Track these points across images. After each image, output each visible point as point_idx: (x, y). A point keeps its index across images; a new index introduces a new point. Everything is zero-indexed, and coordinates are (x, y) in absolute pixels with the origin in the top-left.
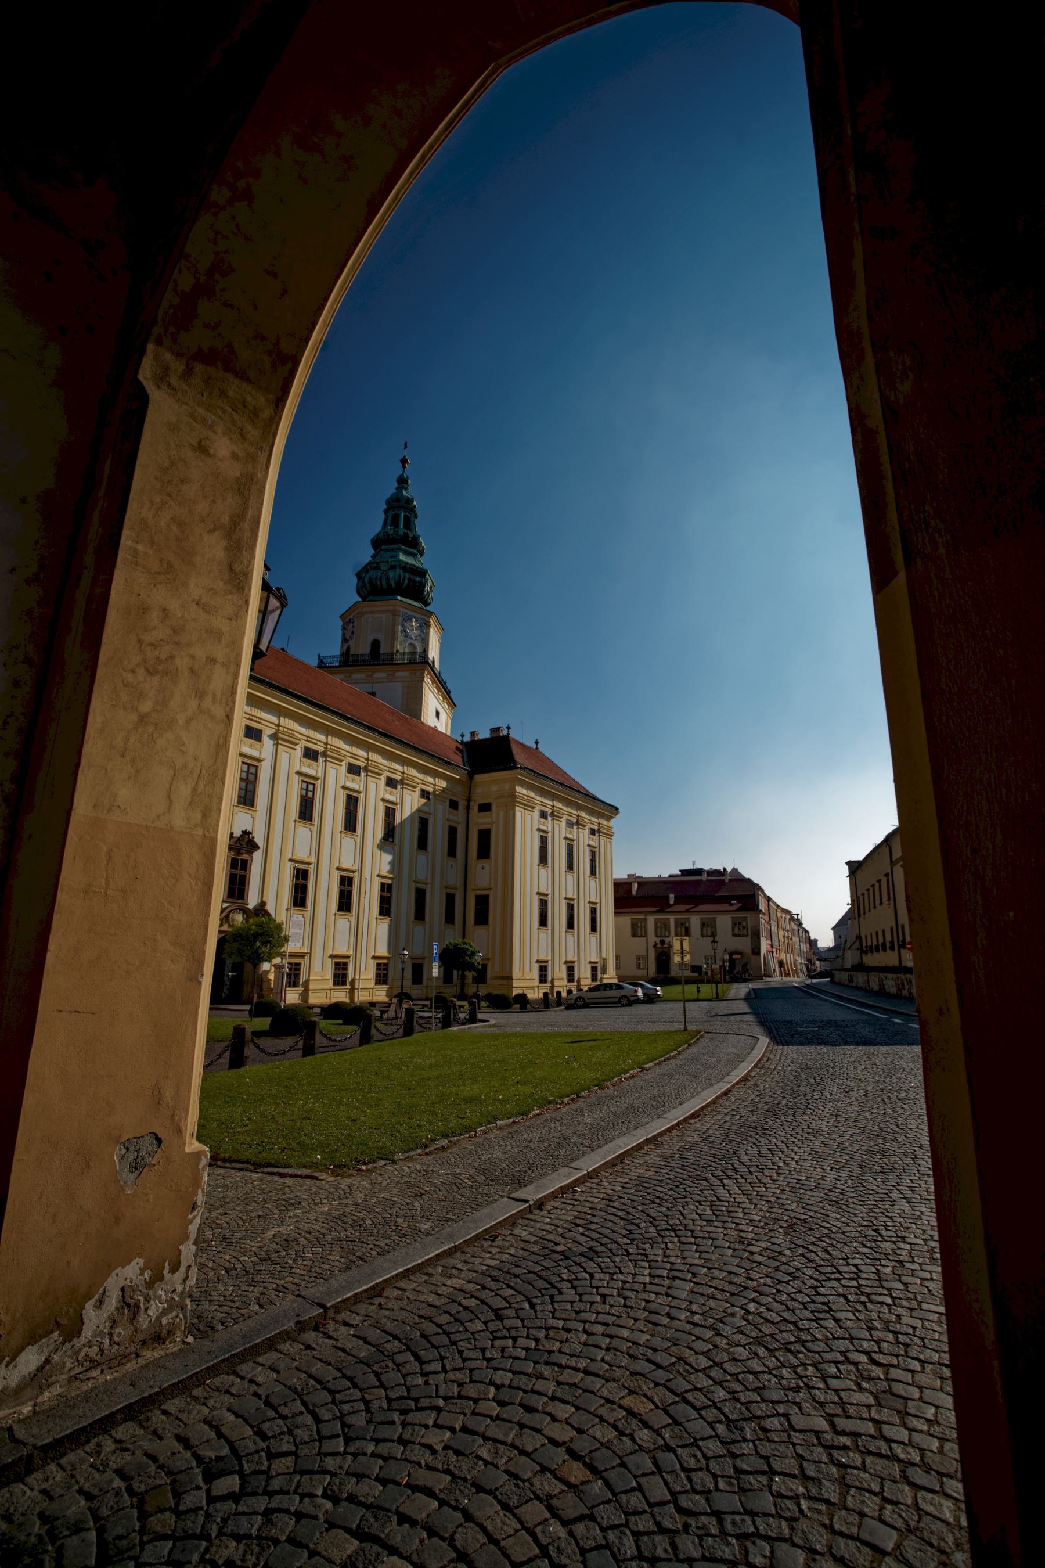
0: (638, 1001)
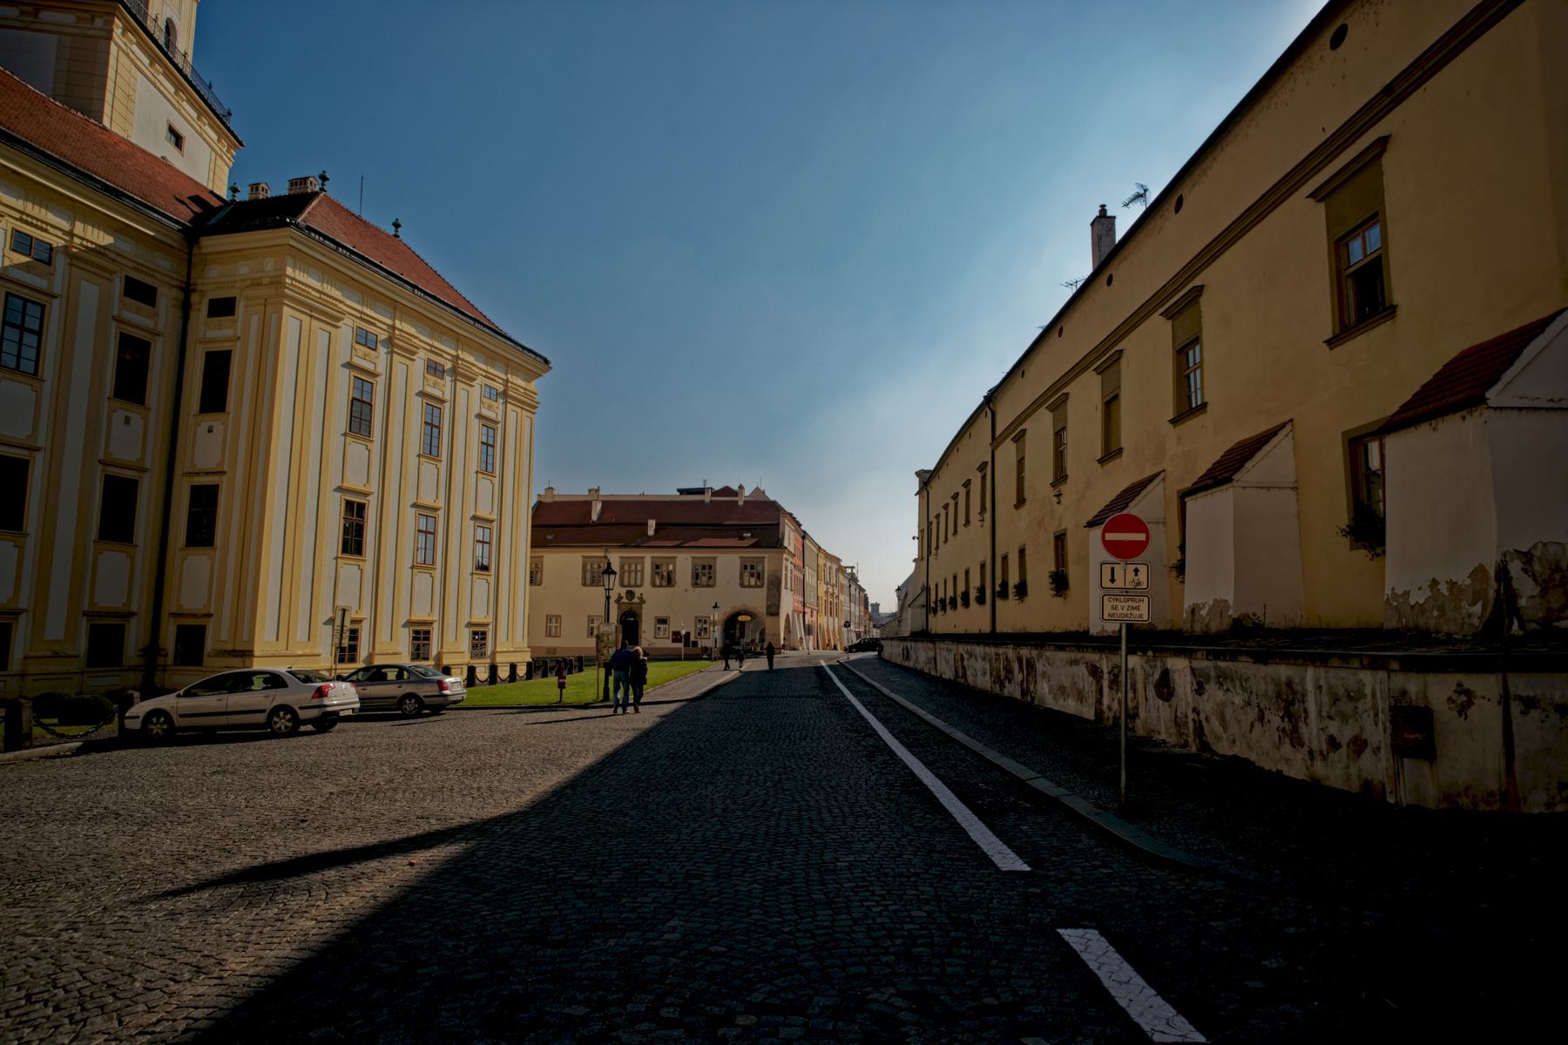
0: (327, 721)
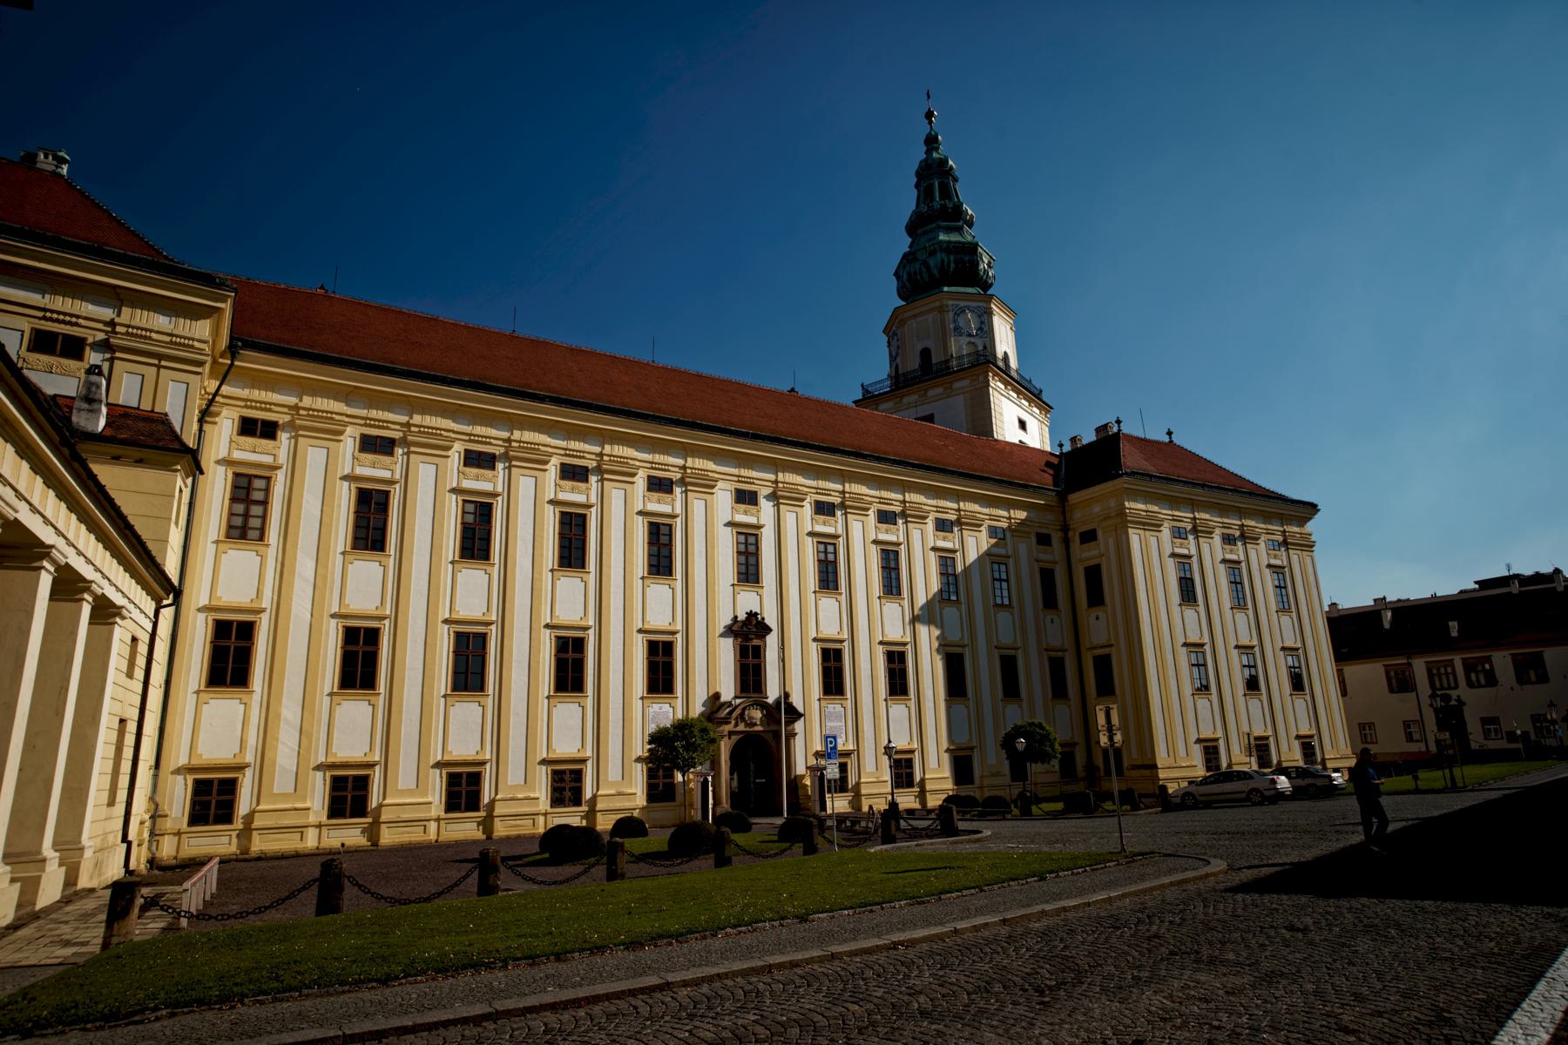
0: (1280, 796)
